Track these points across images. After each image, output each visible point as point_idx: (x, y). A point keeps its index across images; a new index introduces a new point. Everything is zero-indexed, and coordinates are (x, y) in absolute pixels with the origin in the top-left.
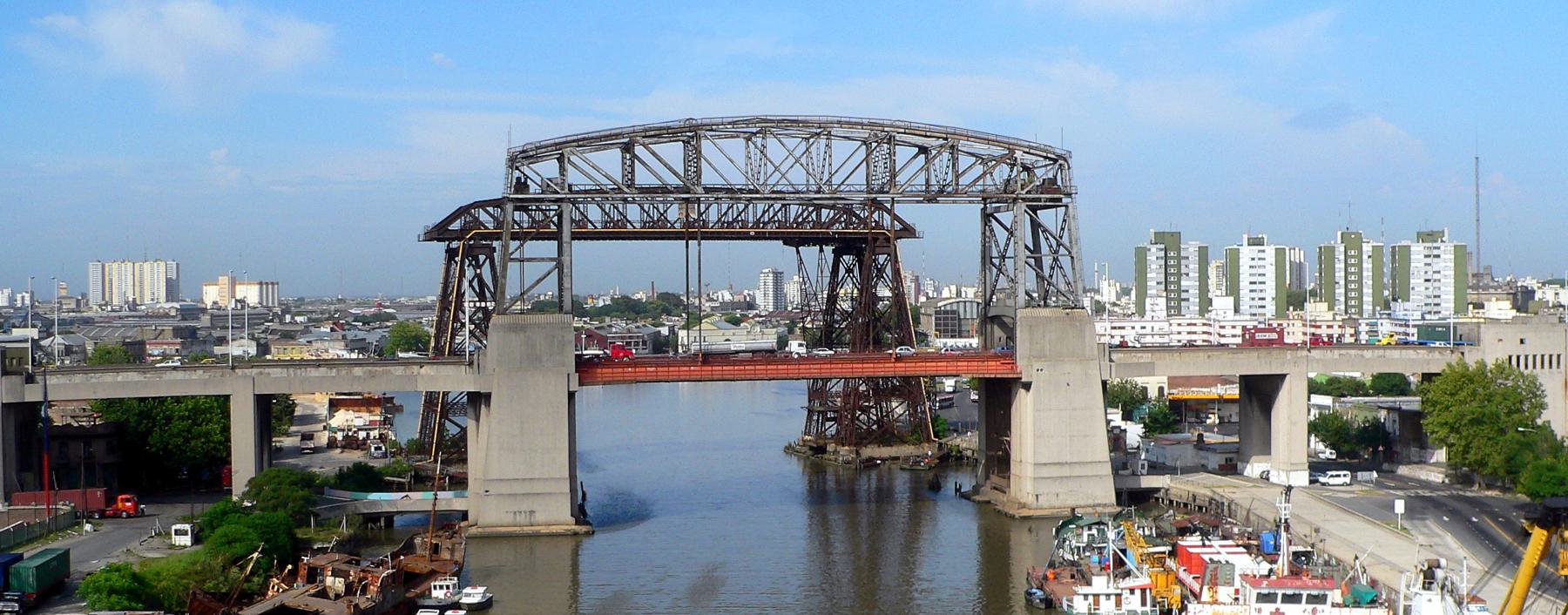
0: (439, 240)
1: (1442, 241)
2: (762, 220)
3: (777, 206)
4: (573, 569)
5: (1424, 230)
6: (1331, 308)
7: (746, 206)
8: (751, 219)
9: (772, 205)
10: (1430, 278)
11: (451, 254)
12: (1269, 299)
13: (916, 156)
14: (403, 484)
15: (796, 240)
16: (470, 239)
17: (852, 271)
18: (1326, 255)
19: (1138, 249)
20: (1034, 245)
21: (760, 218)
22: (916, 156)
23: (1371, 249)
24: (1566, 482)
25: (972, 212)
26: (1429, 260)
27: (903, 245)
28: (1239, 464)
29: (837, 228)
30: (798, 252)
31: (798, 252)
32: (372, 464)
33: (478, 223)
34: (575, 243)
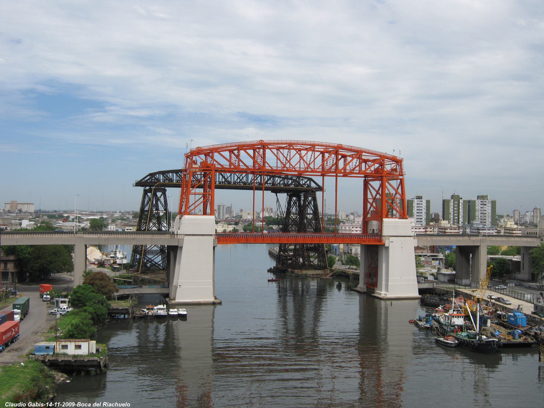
0: (141, 186)
1: (487, 199)
2: (237, 181)
3: (244, 175)
4: (286, 307)
5: (480, 195)
6: (449, 223)
7: (231, 175)
8: (232, 181)
9: (242, 175)
10: (482, 212)
11: (146, 192)
12: (423, 219)
13: (320, 154)
14: (130, 282)
15: (276, 190)
16: (157, 186)
17: (296, 203)
18: (445, 203)
19: (422, 197)
20: (381, 193)
21: (236, 181)
22: (320, 154)
23: (462, 201)
24: (222, 303)
25: (360, 181)
26: (482, 206)
27: (319, 194)
28: (456, 279)
29: (292, 186)
30: (277, 195)
31: (277, 195)
32: (63, 276)
33: (158, 180)
34: (215, 190)
